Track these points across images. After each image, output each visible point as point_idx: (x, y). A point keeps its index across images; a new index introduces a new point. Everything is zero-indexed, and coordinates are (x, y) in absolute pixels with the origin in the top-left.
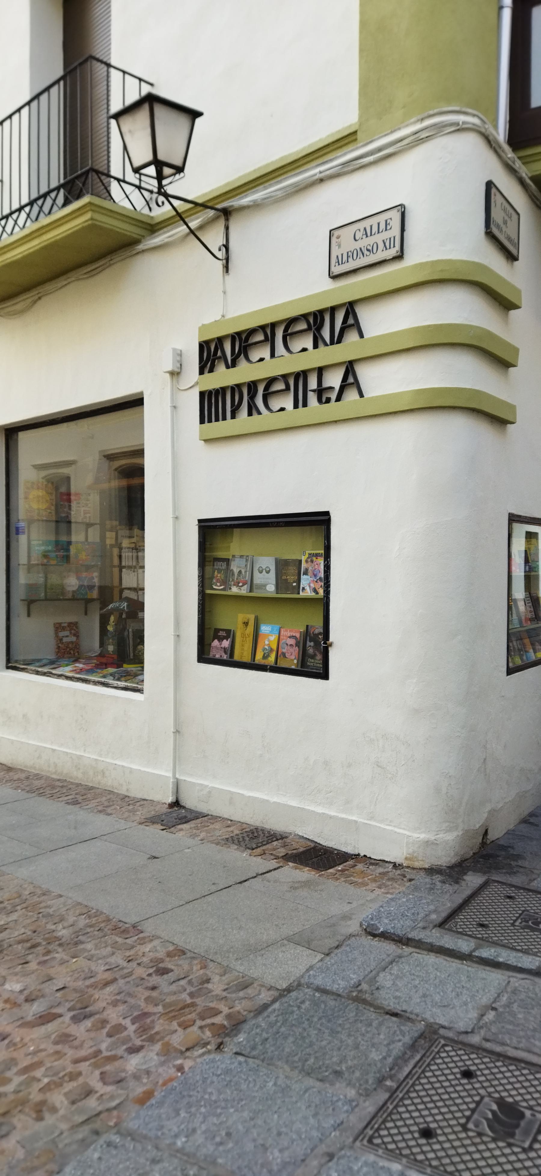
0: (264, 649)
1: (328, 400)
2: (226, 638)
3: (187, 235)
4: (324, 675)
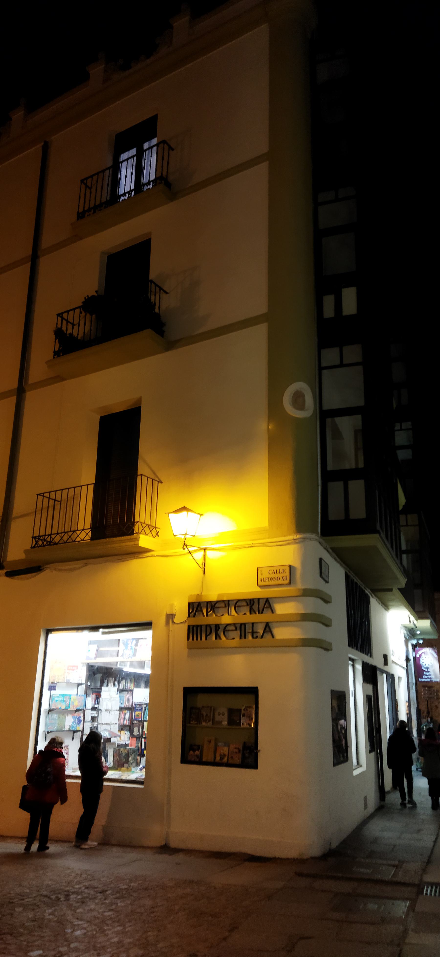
0: (220, 755)
1: (257, 637)
2: (198, 750)
3: (187, 553)
4: (255, 766)
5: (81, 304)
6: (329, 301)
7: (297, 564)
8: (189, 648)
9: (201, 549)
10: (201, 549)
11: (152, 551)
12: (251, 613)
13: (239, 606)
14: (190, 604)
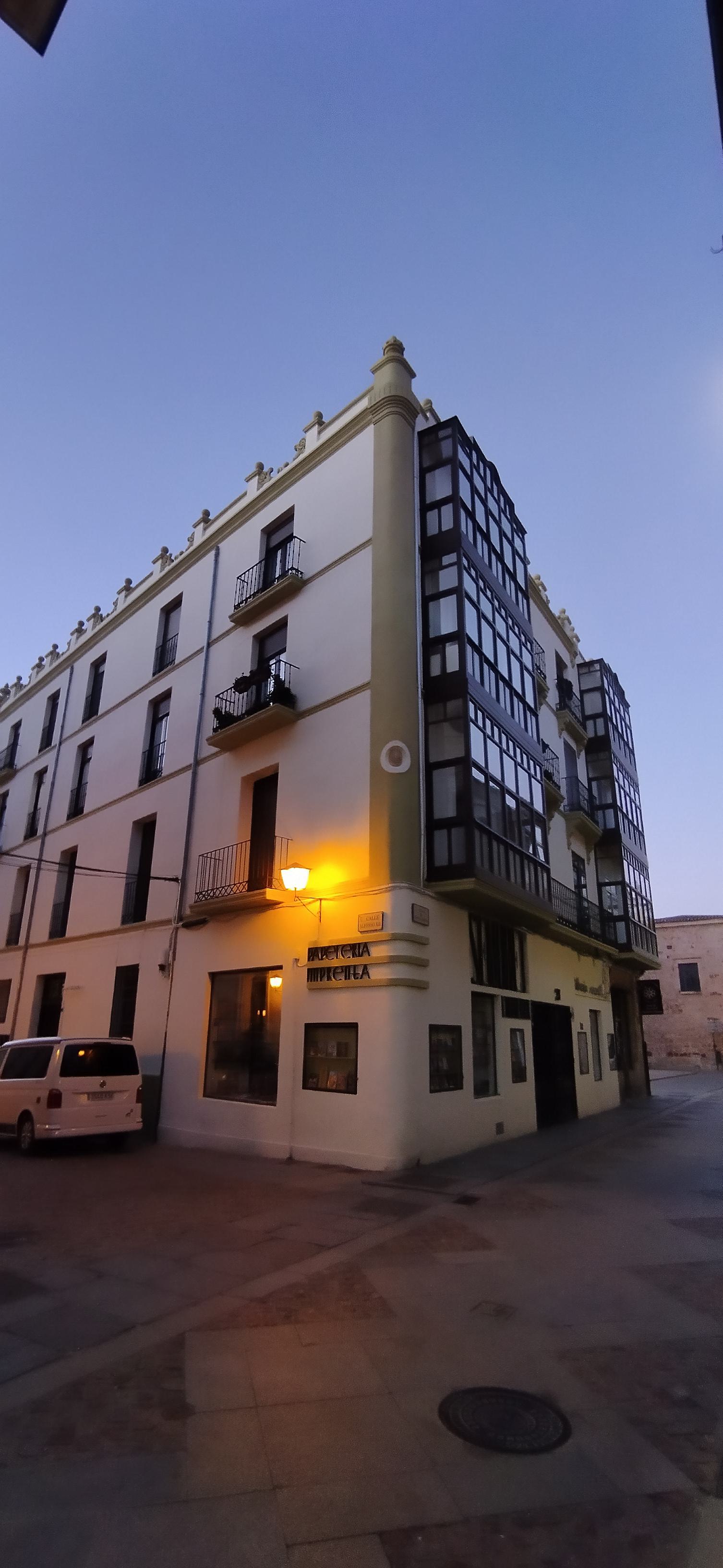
1: (357, 978)
5: (233, 685)
6: (436, 660)
7: (387, 910)
8: (311, 989)
9: (317, 900)
10: (317, 900)
11: (283, 902)
12: (353, 957)
13: (345, 951)
14: (309, 949)
